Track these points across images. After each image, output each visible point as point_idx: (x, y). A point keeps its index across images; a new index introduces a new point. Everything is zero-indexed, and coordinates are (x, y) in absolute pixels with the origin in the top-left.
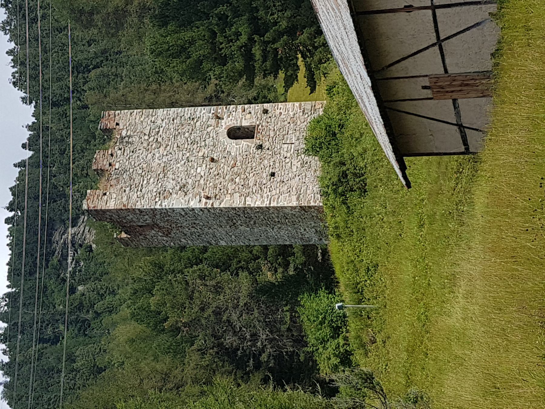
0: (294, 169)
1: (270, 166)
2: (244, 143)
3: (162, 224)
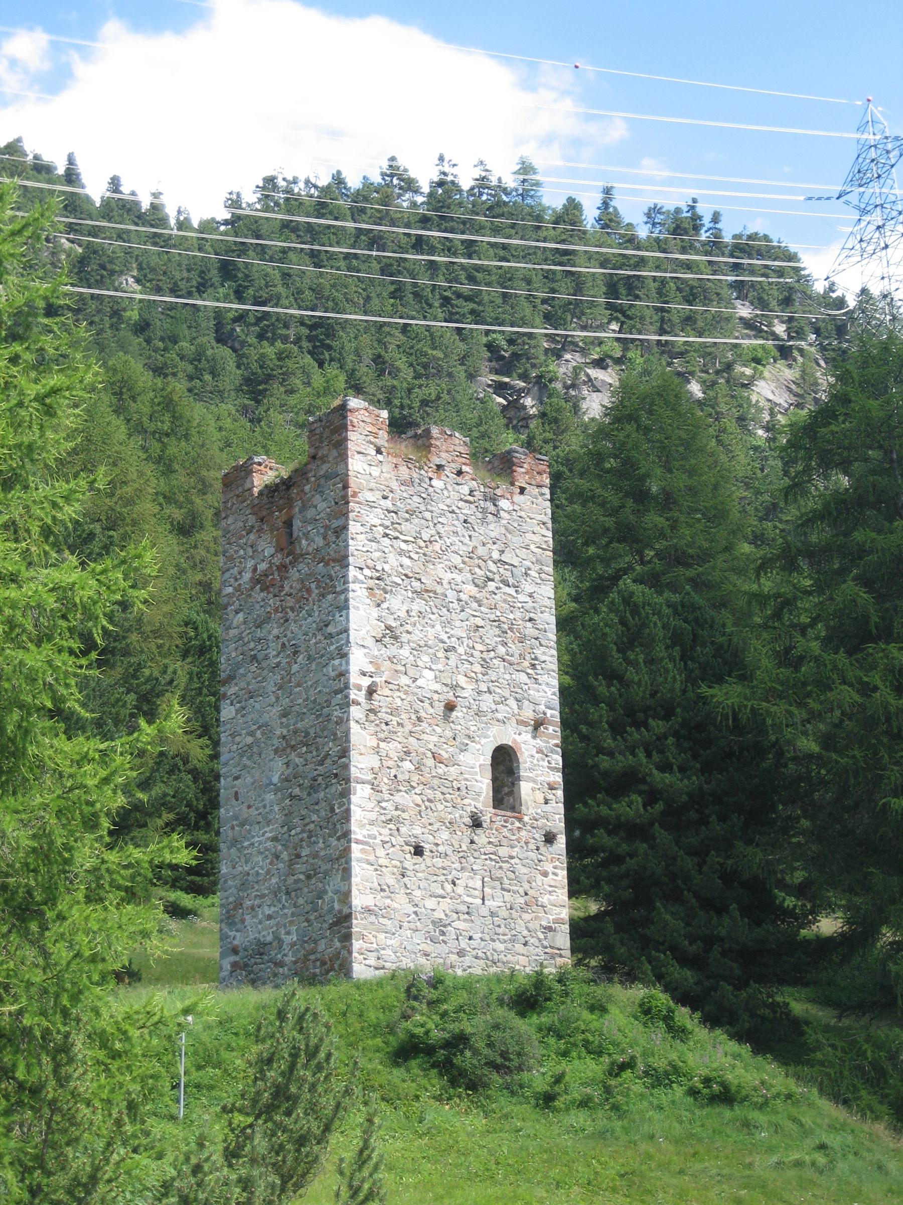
0: (430, 903)
1: (437, 845)
2: (484, 784)
3: (294, 574)
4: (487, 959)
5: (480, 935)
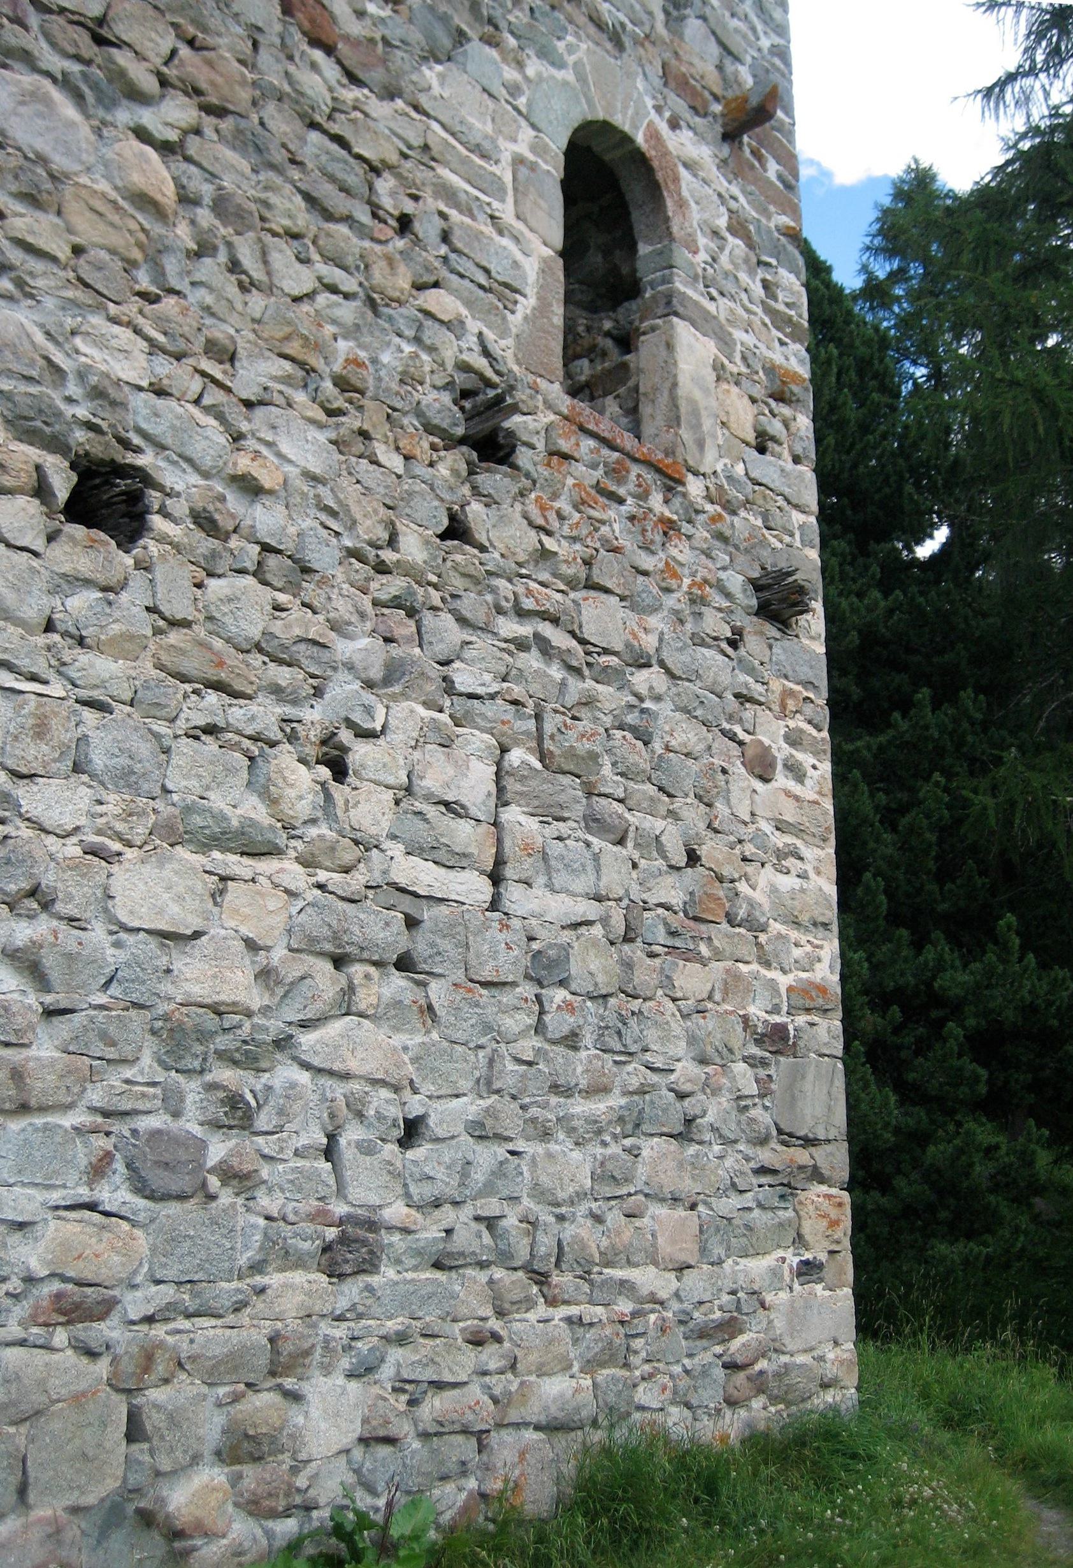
0: (153, 888)
1: (250, 488)
4: (504, 1258)
5: (471, 1107)
